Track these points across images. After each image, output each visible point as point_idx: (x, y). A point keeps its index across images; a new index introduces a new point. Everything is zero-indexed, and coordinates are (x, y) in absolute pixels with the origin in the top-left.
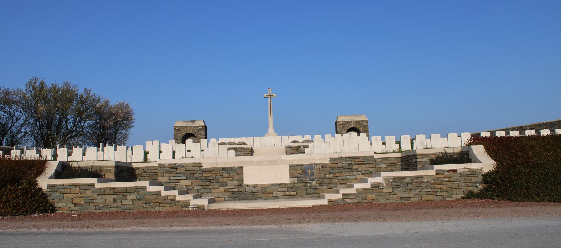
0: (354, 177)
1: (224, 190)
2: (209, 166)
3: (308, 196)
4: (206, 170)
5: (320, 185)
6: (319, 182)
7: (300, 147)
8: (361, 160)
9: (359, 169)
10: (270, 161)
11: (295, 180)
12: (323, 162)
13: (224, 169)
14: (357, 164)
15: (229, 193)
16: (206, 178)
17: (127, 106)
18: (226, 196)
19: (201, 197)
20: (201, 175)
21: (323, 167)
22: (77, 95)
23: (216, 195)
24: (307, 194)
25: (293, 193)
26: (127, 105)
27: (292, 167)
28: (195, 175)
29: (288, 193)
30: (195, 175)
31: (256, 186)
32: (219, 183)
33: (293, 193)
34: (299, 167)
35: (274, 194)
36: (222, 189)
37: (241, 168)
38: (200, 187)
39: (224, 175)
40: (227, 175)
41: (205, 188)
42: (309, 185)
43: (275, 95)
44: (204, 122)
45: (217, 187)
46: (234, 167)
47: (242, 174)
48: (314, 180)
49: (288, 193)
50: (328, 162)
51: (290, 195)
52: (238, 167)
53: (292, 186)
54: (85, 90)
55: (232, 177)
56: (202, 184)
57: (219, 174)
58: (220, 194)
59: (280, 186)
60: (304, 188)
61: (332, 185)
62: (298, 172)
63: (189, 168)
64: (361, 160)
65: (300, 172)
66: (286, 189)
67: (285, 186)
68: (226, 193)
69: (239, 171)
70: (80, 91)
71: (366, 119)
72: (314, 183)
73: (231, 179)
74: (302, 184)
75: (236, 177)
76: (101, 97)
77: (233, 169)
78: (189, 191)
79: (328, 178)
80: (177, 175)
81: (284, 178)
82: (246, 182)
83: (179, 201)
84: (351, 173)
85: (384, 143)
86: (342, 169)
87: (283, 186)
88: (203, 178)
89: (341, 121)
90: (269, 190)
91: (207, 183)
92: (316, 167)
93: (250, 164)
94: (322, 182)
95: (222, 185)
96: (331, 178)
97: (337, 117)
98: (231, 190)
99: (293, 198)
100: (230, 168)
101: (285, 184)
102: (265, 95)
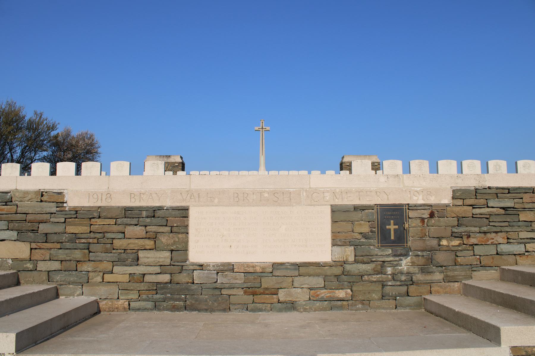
0: (520, 249)
1: (126, 278)
3: (384, 303)
5: (424, 270)
6: (421, 261)
10: (274, 193)
11: (349, 253)
12: (432, 200)
13: (128, 212)
15: (142, 286)
16: (75, 237)
17: (91, 137)
18: (134, 295)
19: (57, 296)
20: (59, 229)
21: (432, 215)
22: (24, 117)
23: (103, 291)
24: (383, 297)
25: (341, 294)
26: (92, 136)
27: (339, 214)
28: (43, 228)
29: (324, 293)
30: (43, 228)
31: (228, 268)
33: (341, 294)
34: (359, 215)
35: (282, 295)
36: (122, 273)
37: (183, 212)
38: (56, 265)
39: (130, 231)
40: (139, 230)
41: (71, 267)
42: (389, 270)
43: (268, 128)
44: (181, 158)
45: (108, 266)
46: (160, 208)
47: (185, 230)
48: (406, 255)
49: (324, 293)
50: (446, 200)
51: (330, 300)
53: (338, 271)
54: (36, 113)
55: (154, 237)
56: (62, 254)
57: (116, 228)
58: (114, 289)
60: (375, 278)
61: (458, 272)
62: (358, 229)
63: (26, 206)
65: (366, 229)
66: (319, 282)
67: (318, 270)
69: (174, 221)
70: (28, 114)
71: (378, 161)
72: (405, 264)
73: (149, 243)
74: (368, 267)
75: (164, 240)
76: (57, 123)
77: (159, 213)
78: (22, 275)
79: (448, 249)
82: (195, 255)
84: (512, 235)
87: (311, 270)
88: (64, 238)
89: (348, 162)
90: (268, 282)
91: (78, 254)
93: (211, 198)
94: (430, 260)
95: (122, 262)
96: (454, 252)
97: (343, 158)
98: (147, 278)
100: (147, 209)
101: (317, 265)
102: (257, 128)
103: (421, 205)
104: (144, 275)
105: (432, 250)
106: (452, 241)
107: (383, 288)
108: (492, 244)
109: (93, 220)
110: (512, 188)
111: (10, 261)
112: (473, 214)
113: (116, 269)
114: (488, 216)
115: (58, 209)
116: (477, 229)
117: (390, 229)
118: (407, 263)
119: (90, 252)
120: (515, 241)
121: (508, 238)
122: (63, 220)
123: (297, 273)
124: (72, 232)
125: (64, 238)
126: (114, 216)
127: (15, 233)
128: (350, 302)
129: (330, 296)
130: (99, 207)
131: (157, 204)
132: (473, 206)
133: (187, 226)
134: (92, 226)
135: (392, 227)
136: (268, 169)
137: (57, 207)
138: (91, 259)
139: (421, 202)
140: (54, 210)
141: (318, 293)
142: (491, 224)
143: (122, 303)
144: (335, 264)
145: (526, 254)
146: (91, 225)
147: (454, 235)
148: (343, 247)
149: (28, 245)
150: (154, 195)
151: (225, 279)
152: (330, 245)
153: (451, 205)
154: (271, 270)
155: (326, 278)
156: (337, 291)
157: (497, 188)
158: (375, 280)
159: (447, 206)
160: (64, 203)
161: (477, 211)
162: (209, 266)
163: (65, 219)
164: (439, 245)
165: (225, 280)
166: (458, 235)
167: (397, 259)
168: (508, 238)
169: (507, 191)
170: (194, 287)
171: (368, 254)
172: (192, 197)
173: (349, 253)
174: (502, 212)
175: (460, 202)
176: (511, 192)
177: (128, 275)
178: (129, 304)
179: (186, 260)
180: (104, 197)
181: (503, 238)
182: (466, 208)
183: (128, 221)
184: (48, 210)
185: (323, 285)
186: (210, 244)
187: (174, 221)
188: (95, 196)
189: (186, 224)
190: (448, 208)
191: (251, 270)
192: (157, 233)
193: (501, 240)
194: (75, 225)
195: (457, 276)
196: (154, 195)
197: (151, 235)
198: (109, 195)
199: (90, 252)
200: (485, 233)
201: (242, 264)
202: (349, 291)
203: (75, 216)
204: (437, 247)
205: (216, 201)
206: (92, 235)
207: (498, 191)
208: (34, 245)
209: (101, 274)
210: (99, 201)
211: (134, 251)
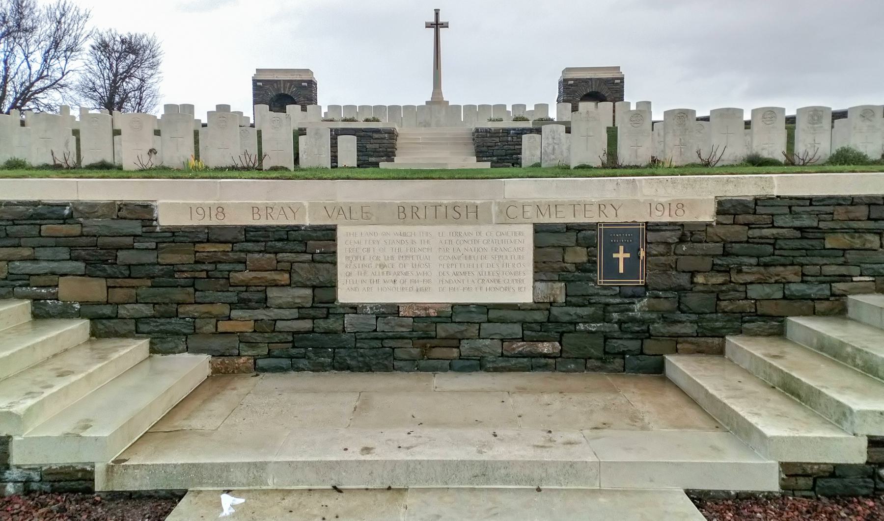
1: (248, 327)
2: (184, 220)
7: (507, 131)
8: (862, 211)
9: (851, 256)
11: (558, 291)
12: (580, 219)
16: (172, 271)
20: (150, 258)
21: (682, 240)
25: (545, 348)
33: (545, 348)
37: (329, 234)
38: (146, 310)
45: (220, 309)
46: (297, 228)
47: (330, 258)
48: (640, 297)
50: (707, 215)
51: (531, 356)
52: (314, 228)
53: (540, 316)
59: (493, 314)
60: (593, 327)
63: (94, 224)
64: (862, 211)
68: (257, 337)
80: (41, 253)
82: (345, 296)
86: (771, 253)
92: (651, 236)
93: (366, 215)
95: (243, 304)
98: (280, 325)
99: (545, 367)
103: (666, 224)
106: (712, 277)
107: (605, 342)
108: (776, 282)
110: (817, 197)
111: (77, 306)
112: (749, 238)
113: (235, 313)
115: (144, 229)
116: (753, 261)
118: (642, 307)
119: (196, 290)
120: (813, 279)
121: (803, 275)
122: (153, 245)
123: (484, 317)
124: (168, 262)
125: (157, 270)
126: (229, 239)
127: (81, 265)
129: (530, 351)
130: (208, 227)
131: (292, 222)
132: (749, 225)
136: (459, 107)
137: (143, 226)
138: (198, 300)
139: (666, 219)
140: (139, 230)
141: (514, 346)
142: (777, 252)
144: (536, 306)
145: (832, 298)
146: (197, 252)
147: (716, 268)
149: (103, 281)
150: (287, 210)
151: (387, 327)
153: (714, 224)
154: (449, 314)
156: (540, 345)
157: (791, 198)
158: (594, 330)
159: (708, 225)
160: (153, 220)
161: (756, 233)
163: (157, 243)
165: (387, 328)
167: (627, 301)
168: (803, 275)
169: (808, 203)
170: (344, 336)
171: (585, 293)
172: (341, 212)
173: (558, 291)
174: (798, 234)
175: (729, 219)
176: (814, 203)
178: (255, 363)
180: (213, 213)
181: (795, 274)
182: (737, 228)
183: (250, 246)
184: (130, 231)
187: (314, 246)
188: (200, 211)
191: (422, 313)
192: (292, 263)
194: (172, 252)
196: (287, 210)
197: (286, 265)
199: (196, 290)
200: (766, 265)
202: (557, 344)
203: (171, 239)
204: (688, 286)
205: (374, 218)
207: (794, 201)
208: (111, 282)
209: (214, 321)
211: (260, 288)
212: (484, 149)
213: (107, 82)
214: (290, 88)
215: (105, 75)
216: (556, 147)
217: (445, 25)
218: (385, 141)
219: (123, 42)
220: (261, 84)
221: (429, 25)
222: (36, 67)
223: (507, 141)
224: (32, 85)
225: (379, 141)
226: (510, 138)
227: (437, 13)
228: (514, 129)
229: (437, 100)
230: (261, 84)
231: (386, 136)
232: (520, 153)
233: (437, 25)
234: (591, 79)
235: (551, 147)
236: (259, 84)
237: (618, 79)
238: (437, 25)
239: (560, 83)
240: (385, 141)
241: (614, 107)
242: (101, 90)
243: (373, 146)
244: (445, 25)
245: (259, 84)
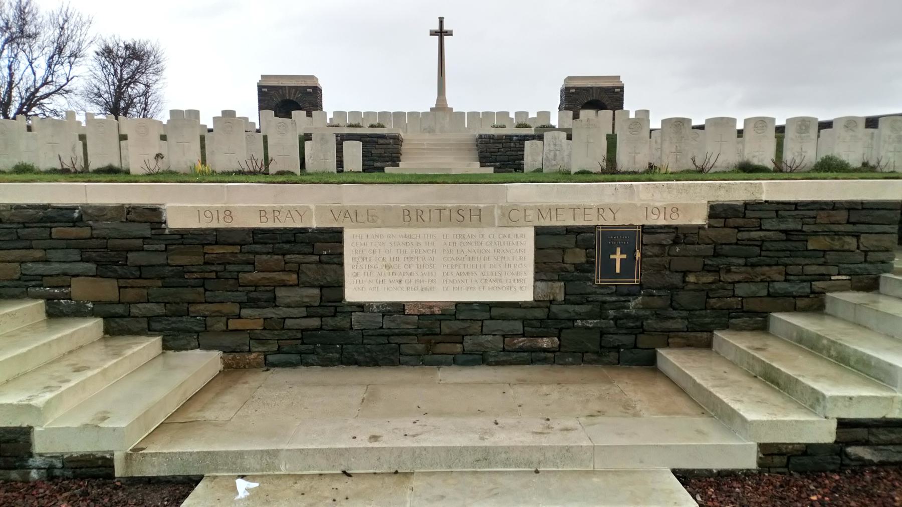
1: (258, 325)
4: (184, 237)
5: (658, 315)
8: (842, 215)
9: (830, 257)
11: (558, 290)
14: (825, 233)
16: (182, 271)
20: (160, 259)
21: (676, 242)
25: (545, 343)
29: (521, 342)
32: (241, 296)
33: (545, 343)
37: (335, 236)
38: (158, 309)
46: (304, 231)
49: (521, 342)
50: (699, 219)
53: (539, 314)
60: (590, 323)
62: (569, 259)
63: (104, 227)
66: (518, 326)
68: (267, 334)
80: (52, 254)
81: (512, 279)
82: (352, 294)
83: (361, 307)
85: (123, 137)
92: (647, 239)
93: (371, 217)
95: (252, 303)
98: (289, 323)
99: (544, 361)
103: (662, 227)
104: (284, 319)
105: (673, 288)
106: (703, 276)
107: (601, 337)
108: (762, 281)
109: (206, 247)
111: (90, 305)
113: (244, 312)
114: (759, 243)
115: (153, 232)
116: (741, 261)
117: (615, 260)
119: (206, 290)
121: (787, 274)
122: (163, 247)
123: (487, 315)
124: (178, 263)
126: (238, 241)
127: (92, 267)
128: (558, 354)
129: (530, 346)
132: (739, 228)
133: (341, 255)
134: (206, 256)
135: (618, 256)
137: (152, 229)
140: (148, 233)
142: (763, 253)
143: (19, 484)
146: (206, 253)
147: (706, 268)
148: (550, 283)
149: (114, 283)
150: (294, 213)
152: (532, 280)
155: (524, 321)
156: (540, 340)
157: (778, 203)
159: (700, 228)
162: (372, 306)
163: (166, 245)
164: (684, 282)
165: (393, 325)
166: (713, 269)
168: (787, 274)
170: (351, 333)
172: (347, 215)
174: (783, 236)
175: (719, 223)
177: (262, 320)
179: (342, 298)
180: (221, 216)
181: (779, 273)
182: (728, 231)
183: (258, 247)
185: (521, 332)
186: (370, 279)
189: (339, 251)
190: (701, 232)
192: (300, 264)
193: (776, 277)
195: (707, 324)
196: (294, 213)
197: (294, 267)
198: (227, 213)
199: (206, 290)
201: (416, 304)
202: (556, 339)
203: (180, 241)
204: (681, 284)
205: (379, 221)
206: (209, 268)
208: (122, 282)
209: (224, 319)
210: (215, 221)
212: (488, 154)
213: (112, 87)
214: (295, 94)
215: (110, 80)
216: (558, 153)
217: (450, 33)
218: (390, 147)
219: (127, 47)
220: (266, 90)
221: (433, 33)
222: (41, 73)
223: (510, 147)
224: (37, 90)
225: (384, 146)
226: (512, 145)
227: (441, 21)
228: (517, 136)
229: (441, 107)
230: (266, 90)
231: (391, 141)
232: (523, 159)
233: (441, 33)
234: (592, 88)
235: (552, 154)
236: (264, 90)
237: (618, 88)
238: (441, 33)
239: (562, 91)
240: (390, 147)
241: (614, 114)
242: (106, 96)
243: (379, 151)
244: (450, 33)
245: (264, 90)
